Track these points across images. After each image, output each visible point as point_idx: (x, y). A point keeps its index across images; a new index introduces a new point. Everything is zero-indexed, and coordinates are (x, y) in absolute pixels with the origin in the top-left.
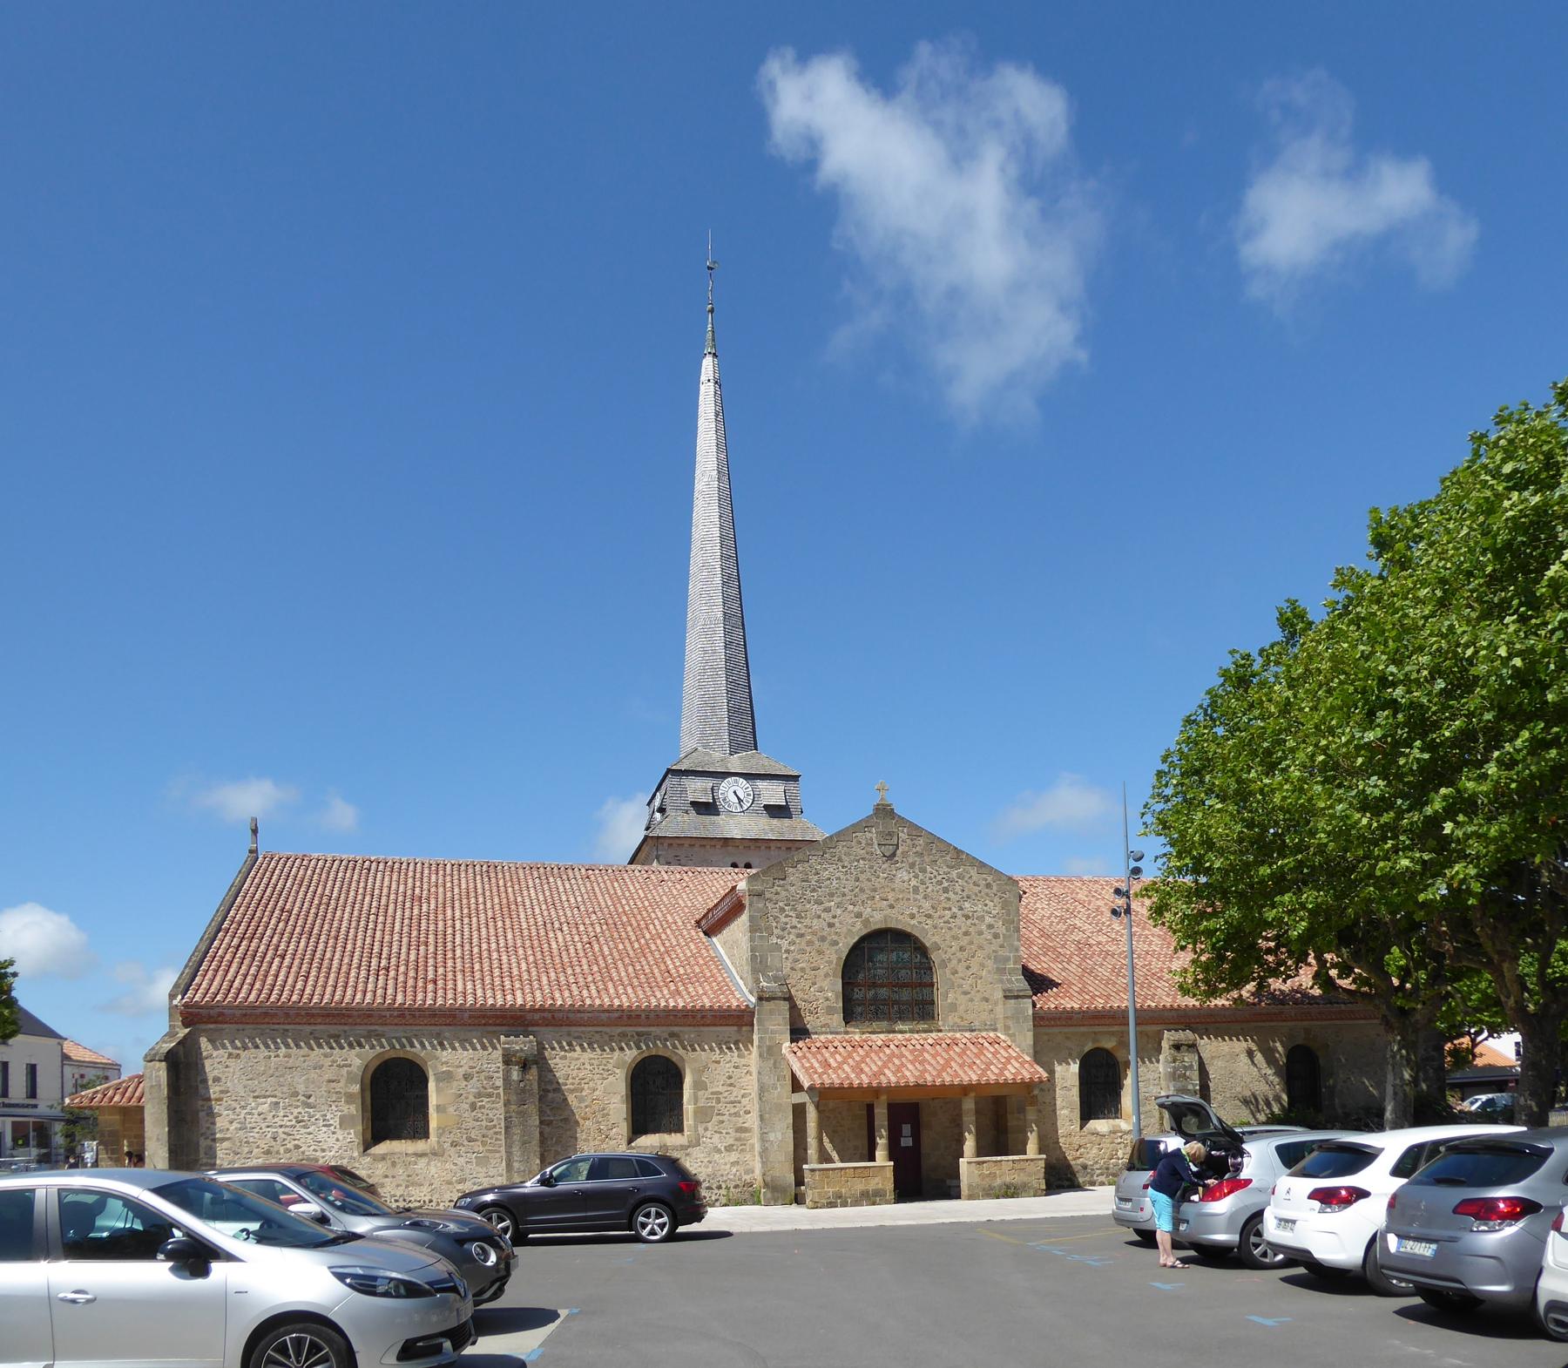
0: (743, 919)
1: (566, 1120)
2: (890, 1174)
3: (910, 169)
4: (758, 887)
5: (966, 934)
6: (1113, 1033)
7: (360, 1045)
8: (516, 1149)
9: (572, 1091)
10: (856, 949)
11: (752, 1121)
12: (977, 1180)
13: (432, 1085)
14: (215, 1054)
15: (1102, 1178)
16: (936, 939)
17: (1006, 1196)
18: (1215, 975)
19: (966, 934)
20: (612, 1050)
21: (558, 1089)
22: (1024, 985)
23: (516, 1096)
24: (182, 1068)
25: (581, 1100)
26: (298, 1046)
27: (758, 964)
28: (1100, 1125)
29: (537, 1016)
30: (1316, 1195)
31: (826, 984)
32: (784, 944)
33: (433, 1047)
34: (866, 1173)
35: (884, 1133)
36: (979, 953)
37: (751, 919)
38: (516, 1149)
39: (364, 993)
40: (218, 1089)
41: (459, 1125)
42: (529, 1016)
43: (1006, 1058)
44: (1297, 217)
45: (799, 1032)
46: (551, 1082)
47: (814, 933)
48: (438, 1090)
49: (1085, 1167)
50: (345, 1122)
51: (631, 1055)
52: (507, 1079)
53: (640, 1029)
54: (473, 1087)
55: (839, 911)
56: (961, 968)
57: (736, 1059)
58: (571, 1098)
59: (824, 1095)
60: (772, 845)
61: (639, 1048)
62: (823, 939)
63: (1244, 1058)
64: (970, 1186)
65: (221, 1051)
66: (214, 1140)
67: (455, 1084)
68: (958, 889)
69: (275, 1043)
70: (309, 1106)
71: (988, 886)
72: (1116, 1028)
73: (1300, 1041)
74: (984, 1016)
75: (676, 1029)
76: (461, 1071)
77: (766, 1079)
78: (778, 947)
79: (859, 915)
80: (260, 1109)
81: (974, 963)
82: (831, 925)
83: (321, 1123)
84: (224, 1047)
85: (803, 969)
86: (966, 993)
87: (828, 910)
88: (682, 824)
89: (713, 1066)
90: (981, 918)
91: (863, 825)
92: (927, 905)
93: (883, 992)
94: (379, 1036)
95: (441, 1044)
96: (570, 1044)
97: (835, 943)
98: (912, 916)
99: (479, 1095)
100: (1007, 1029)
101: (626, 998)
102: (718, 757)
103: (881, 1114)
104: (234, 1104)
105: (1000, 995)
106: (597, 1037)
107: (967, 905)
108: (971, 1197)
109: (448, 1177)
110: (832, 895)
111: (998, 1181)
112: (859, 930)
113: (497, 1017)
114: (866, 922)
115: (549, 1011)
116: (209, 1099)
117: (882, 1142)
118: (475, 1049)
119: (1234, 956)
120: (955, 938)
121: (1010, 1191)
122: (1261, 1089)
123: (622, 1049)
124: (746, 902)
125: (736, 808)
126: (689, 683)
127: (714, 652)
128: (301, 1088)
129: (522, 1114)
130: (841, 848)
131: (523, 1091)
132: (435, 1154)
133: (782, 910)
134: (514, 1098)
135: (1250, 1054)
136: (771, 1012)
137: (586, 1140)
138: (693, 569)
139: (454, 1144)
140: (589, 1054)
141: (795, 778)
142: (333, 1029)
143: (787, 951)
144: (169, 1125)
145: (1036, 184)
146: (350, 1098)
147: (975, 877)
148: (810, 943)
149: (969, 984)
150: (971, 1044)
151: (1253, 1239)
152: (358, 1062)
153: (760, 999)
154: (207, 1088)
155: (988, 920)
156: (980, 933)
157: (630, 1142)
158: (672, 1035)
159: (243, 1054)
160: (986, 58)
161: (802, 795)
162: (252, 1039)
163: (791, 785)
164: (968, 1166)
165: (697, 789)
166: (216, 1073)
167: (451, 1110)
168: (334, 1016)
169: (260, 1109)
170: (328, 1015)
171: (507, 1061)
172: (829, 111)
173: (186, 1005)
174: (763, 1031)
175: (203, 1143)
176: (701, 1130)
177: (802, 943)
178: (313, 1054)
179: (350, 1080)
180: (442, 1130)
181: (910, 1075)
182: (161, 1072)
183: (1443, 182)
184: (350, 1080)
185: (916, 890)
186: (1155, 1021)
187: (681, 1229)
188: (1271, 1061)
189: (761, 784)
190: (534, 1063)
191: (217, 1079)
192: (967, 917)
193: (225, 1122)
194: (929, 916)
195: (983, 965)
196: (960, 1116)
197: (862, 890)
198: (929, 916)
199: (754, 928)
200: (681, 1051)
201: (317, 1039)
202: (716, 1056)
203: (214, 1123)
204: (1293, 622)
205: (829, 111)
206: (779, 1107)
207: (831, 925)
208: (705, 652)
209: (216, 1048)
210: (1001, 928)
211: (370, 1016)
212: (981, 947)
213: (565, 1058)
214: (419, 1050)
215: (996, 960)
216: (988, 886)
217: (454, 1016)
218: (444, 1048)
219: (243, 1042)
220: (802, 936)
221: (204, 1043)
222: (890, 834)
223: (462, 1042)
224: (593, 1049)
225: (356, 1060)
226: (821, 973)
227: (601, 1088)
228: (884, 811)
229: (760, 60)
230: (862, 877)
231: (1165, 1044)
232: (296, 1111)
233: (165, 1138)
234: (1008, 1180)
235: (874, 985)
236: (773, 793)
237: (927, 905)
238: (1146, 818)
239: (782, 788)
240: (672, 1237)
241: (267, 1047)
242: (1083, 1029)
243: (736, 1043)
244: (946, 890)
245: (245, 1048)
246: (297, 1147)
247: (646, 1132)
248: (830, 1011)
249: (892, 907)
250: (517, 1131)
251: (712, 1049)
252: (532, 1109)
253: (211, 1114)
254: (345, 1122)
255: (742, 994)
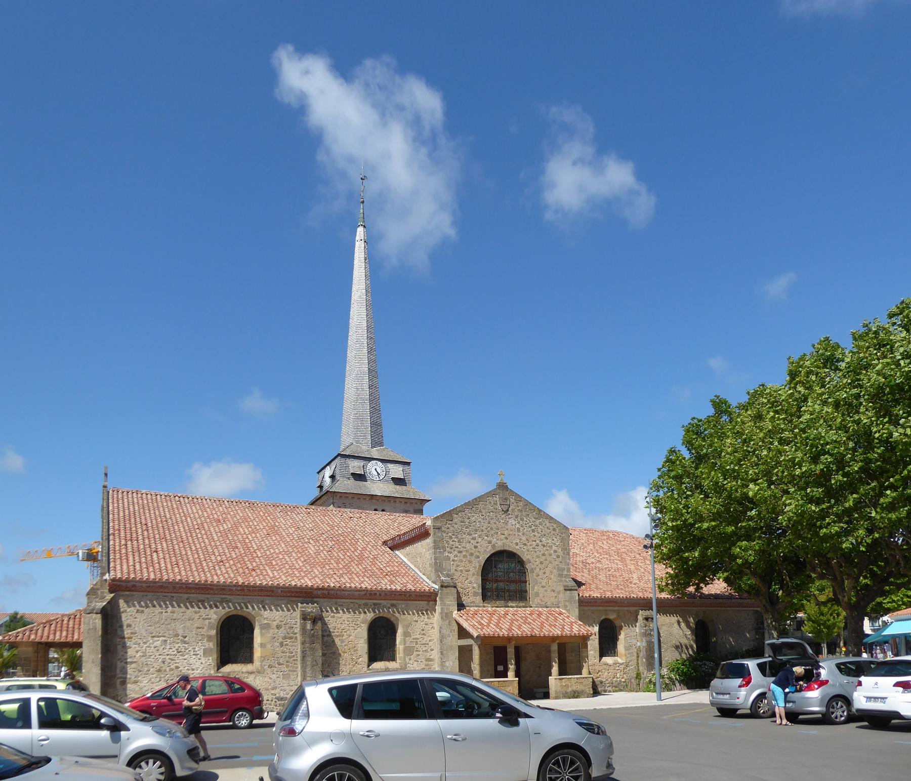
0: (429, 541)
1: (334, 653)
2: (516, 685)
3: (358, 121)
4: (438, 524)
5: (543, 555)
6: (614, 611)
7: (217, 607)
8: (308, 670)
9: (337, 636)
10: (488, 560)
11: (435, 655)
12: (559, 689)
13: (257, 632)
14: (128, 610)
15: (610, 689)
16: (529, 557)
17: (574, 697)
18: (679, 581)
19: (543, 555)
20: (360, 613)
21: (330, 635)
22: (574, 584)
23: (309, 639)
24: (110, 619)
25: (342, 641)
26: (179, 606)
27: (438, 567)
28: (608, 660)
29: (319, 592)
30: (897, 684)
31: (473, 579)
32: (452, 556)
33: (259, 609)
34: (504, 684)
35: (513, 662)
36: (550, 566)
37: (435, 542)
38: (308, 670)
39: (221, 576)
40: (129, 631)
41: (273, 655)
42: (315, 592)
43: (567, 623)
44: (574, 180)
45: (461, 606)
46: (326, 631)
47: (467, 551)
48: (262, 634)
49: (601, 682)
50: (206, 653)
51: (370, 616)
52: (303, 629)
53: (375, 601)
54: (282, 633)
55: (480, 540)
56: (541, 573)
57: (426, 620)
58: (337, 641)
59: (483, 641)
60: (398, 500)
61: (374, 612)
62: (472, 554)
63: (676, 625)
64: (556, 692)
65: (132, 609)
66: (126, 663)
67: (271, 631)
68: (539, 530)
69: (166, 604)
70: (185, 643)
71: (554, 530)
72: (616, 608)
73: (701, 618)
74: (553, 600)
75: (395, 602)
76: (275, 623)
77: (444, 631)
78: (448, 558)
79: (490, 542)
80: (155, 644)
81: (548, 571)
82: (476, 547)
83: (192, 653)
84: (134, 606)
85: (461, 571)
86: (543, 587)
87: (474, 539)
88: (346, 485)
89: (414, 623)
90: (551, 547)
91: (491, 494)
92: (524, 538)
93: (501, 585)
94: (228, 602)
95: (264, 607)
96: (336, 609)
97: (478, 557)
98: (517, 544)
99: (285, 638)
100: (565, 607)
101: (367, 584)
102: (365, 449)
103: (511, 652)
104: (140, 641)
105: (562, 588)
106: (352, 605)
107: (544, 539)
108: (556, 698)
109: (266, 686)
110: (476, 530)
111: (570, 689)
112: (490, 551)
113: (297, 592)
114: (494, 546)
115: (327, 589)
116: (124, 638)
117: (512, 667)
118: (283, 611)
119: (688, 573)
120: (538, 557)
121: (576, 695)
122: (684, 641)
123: (365, 613)
124: (431, 532)
125: (376, 478)
126: (347, 406)
127: (363, 390)
128: (180, 632)
129: (313, 649)
130: (481, 505)
131: (313, 636)
132: (259, 672)
133: (451, 537)
134: (308, 640)
135: (679, 622)
136: (448, 594)
137: (345, 665)
138: (350, 343)
139: (270, 666)
140: (347, 615)
141: (408, 464)
142: (201, 597)
143: (453, 560)
144: (102, 653)
145: (423, 138)
146: (209, 638)
147: (548, 524)
148: (465, 556)
149: (542, 582)
150: (545, 614)
151: (831, 710)
152: (215, 617)
153: (442, 586)
154: (123, 631)
155: (554, 548)
156: (550, 555)
157: (369, 666)
158: (393, 605)
159: (146, 610)
160: (403, 69)
161: (413, 474)
162: (151, 601)
163: (406, 467)
164: (554, 680)
165: (355, 466)
166: (128, 622)
167: (269, 646)
168: (202, 589)
169: (155, 644)
170: (199, 588)
171: (304, 617)
172: (309, 80)
173: (114, 580)
174: (443, 604)
175: (119, 665)
176: (407, 659)
177: (461, 556)
178: (188, 612)
179: (210, 628)
180: (263, 658)
181: (526, 630)
182: (97, 621)
183: (640, 174)
184: (210, 628)
185: (519, 530)
186: (646, 604)
187: (255, 722)
188: (688, 626)
189: (390, 466)
190: (317, 619)
191: (129, 626)
192: (544, 546)
193: (134, 651)
194: (525, 545)
195: (551, 572)
196: (550, 652)
197: (492, 529)
198: (525, 545)
199: (436, 546)
200: (397, 615)
201: (191, 603)
202: (416, 618)
203: (126, 653)
204: (721, 406)
205: (309, 80)
206: (451, 647)
207: (476, 547)
208: (358, 389)
209: (129, 607)
210: (560, 553)
211: (223, 589)
212: (550, 562)
213: (333, 617)
214: (251, 610)
215: (559, 570)
216: (554, 530)
217: (273, 591)
218: (265, 610)
219: (146, 603)
220: (460, 552)
221: (122, 603)
222: (506, 499)
223: (276, 606)
224: (349, 612)
225: (214, 615)
226: (471, 573)
227: (353, 635)
228: (502, 487)
229: (274, 47)
230: (492, 522)
231: (640, 617)
232: (177, 646)
233: (99, 661)
234: (575, 688)
235: (497, 581)
236: (397, 471)
237: (524, 538)
238: (648, 499)
239: (401, 469)
240: (251, 726)
241: (161, 606)
242: (601, 608)
243: (426, 611)
244: (533, 531)
245: (147, 607)
246: (177, 667)
247: (376, 661)
248: (475, 594)
249: (506, 538)
250: (309, 659)
251: (413, 614)
252: (318, 645)
253: (125, 647)
254: (206, 653)
255: (428, 584)
